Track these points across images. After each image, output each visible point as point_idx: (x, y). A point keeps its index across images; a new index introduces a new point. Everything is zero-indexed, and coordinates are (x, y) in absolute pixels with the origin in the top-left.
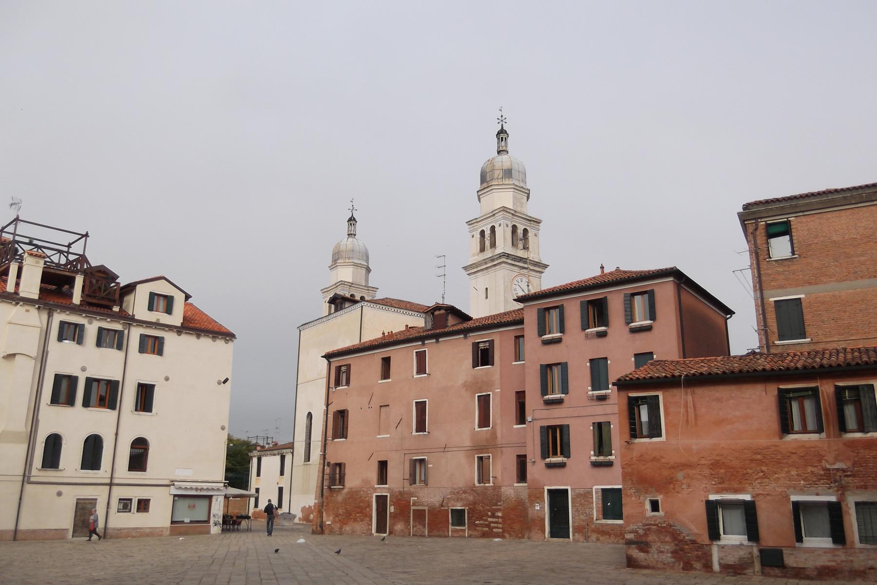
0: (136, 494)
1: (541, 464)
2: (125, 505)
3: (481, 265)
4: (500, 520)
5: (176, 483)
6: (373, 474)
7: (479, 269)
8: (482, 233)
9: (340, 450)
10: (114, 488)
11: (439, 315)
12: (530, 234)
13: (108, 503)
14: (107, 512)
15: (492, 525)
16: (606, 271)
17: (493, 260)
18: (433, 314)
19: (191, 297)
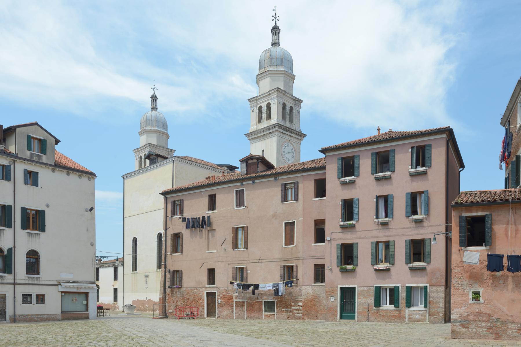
0: (35, 291)
1: (371, 269)
2: (26, 298)
3: (259, 133)
4: (301, 308)
5: (62, 284)
6: (204, 277)
7: (258, 135)
8: (260, 109)
9: (175, 262)
10: (12, 286)
11: (252, 163)
12: (294, 111)
13: (15, 297)
14: (15, 304)
15: (295, 311)
16: (382, 132)
17: (269, 129)
18: (247, 163)
19: (60, 141)
